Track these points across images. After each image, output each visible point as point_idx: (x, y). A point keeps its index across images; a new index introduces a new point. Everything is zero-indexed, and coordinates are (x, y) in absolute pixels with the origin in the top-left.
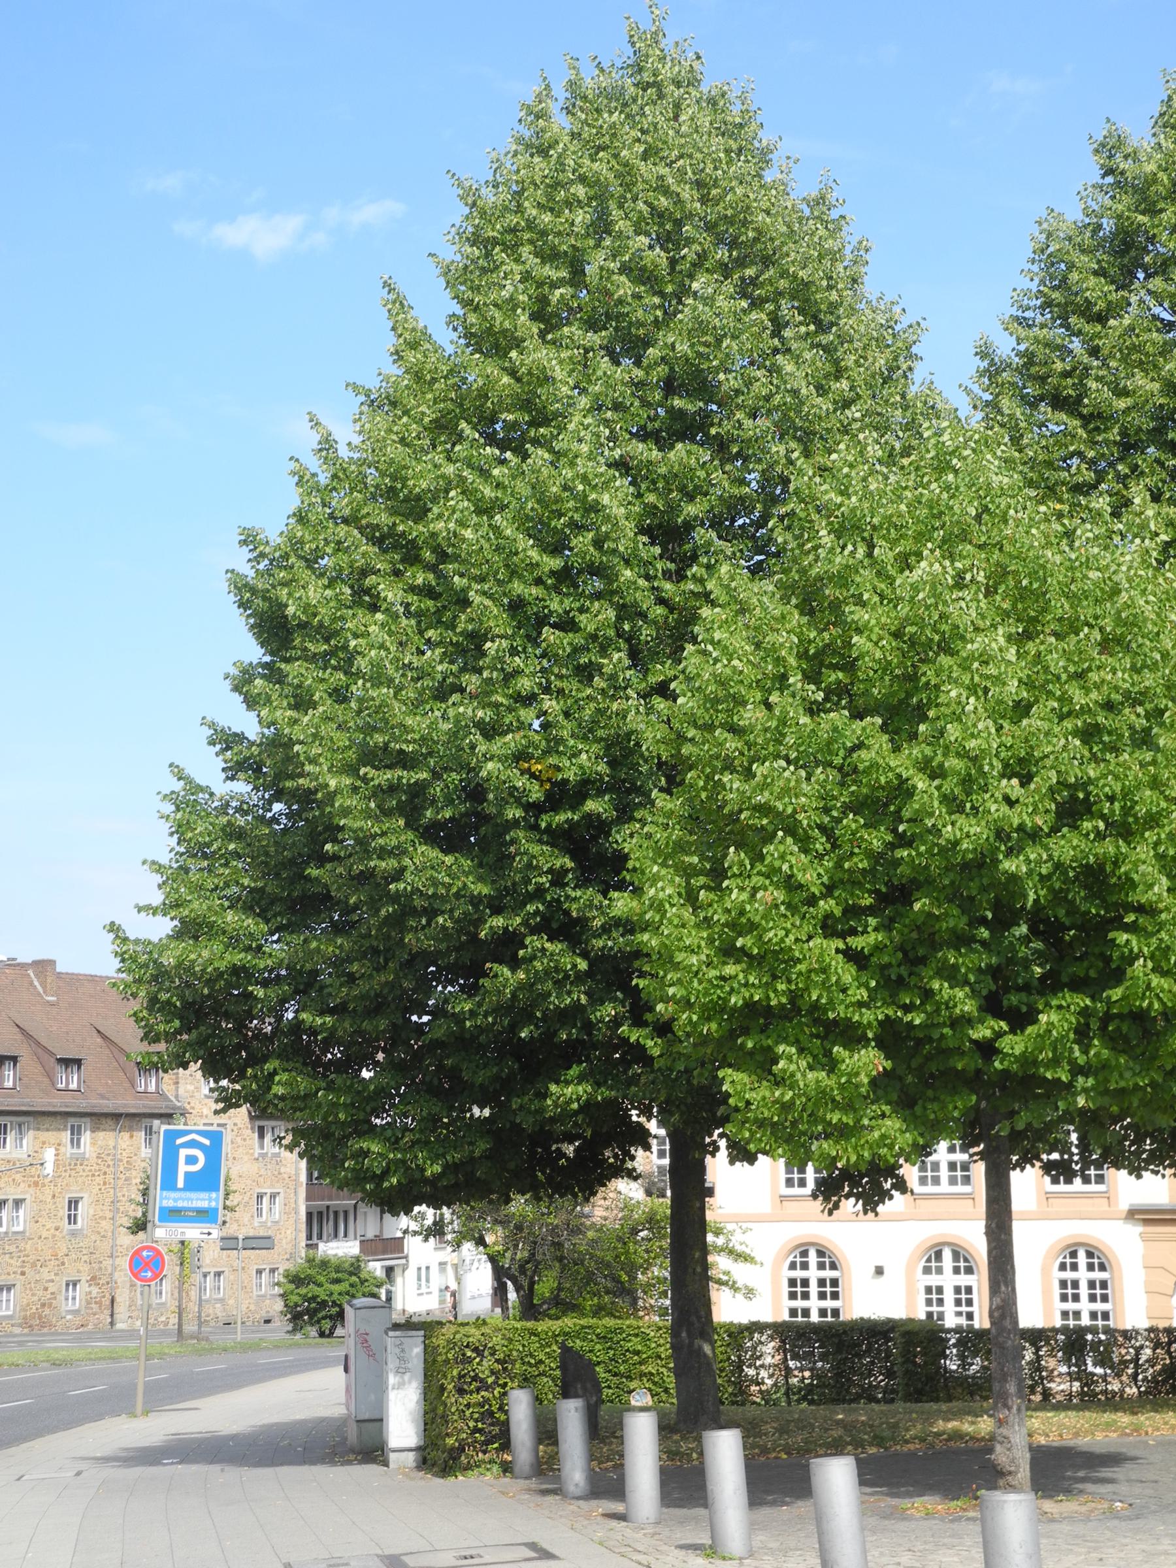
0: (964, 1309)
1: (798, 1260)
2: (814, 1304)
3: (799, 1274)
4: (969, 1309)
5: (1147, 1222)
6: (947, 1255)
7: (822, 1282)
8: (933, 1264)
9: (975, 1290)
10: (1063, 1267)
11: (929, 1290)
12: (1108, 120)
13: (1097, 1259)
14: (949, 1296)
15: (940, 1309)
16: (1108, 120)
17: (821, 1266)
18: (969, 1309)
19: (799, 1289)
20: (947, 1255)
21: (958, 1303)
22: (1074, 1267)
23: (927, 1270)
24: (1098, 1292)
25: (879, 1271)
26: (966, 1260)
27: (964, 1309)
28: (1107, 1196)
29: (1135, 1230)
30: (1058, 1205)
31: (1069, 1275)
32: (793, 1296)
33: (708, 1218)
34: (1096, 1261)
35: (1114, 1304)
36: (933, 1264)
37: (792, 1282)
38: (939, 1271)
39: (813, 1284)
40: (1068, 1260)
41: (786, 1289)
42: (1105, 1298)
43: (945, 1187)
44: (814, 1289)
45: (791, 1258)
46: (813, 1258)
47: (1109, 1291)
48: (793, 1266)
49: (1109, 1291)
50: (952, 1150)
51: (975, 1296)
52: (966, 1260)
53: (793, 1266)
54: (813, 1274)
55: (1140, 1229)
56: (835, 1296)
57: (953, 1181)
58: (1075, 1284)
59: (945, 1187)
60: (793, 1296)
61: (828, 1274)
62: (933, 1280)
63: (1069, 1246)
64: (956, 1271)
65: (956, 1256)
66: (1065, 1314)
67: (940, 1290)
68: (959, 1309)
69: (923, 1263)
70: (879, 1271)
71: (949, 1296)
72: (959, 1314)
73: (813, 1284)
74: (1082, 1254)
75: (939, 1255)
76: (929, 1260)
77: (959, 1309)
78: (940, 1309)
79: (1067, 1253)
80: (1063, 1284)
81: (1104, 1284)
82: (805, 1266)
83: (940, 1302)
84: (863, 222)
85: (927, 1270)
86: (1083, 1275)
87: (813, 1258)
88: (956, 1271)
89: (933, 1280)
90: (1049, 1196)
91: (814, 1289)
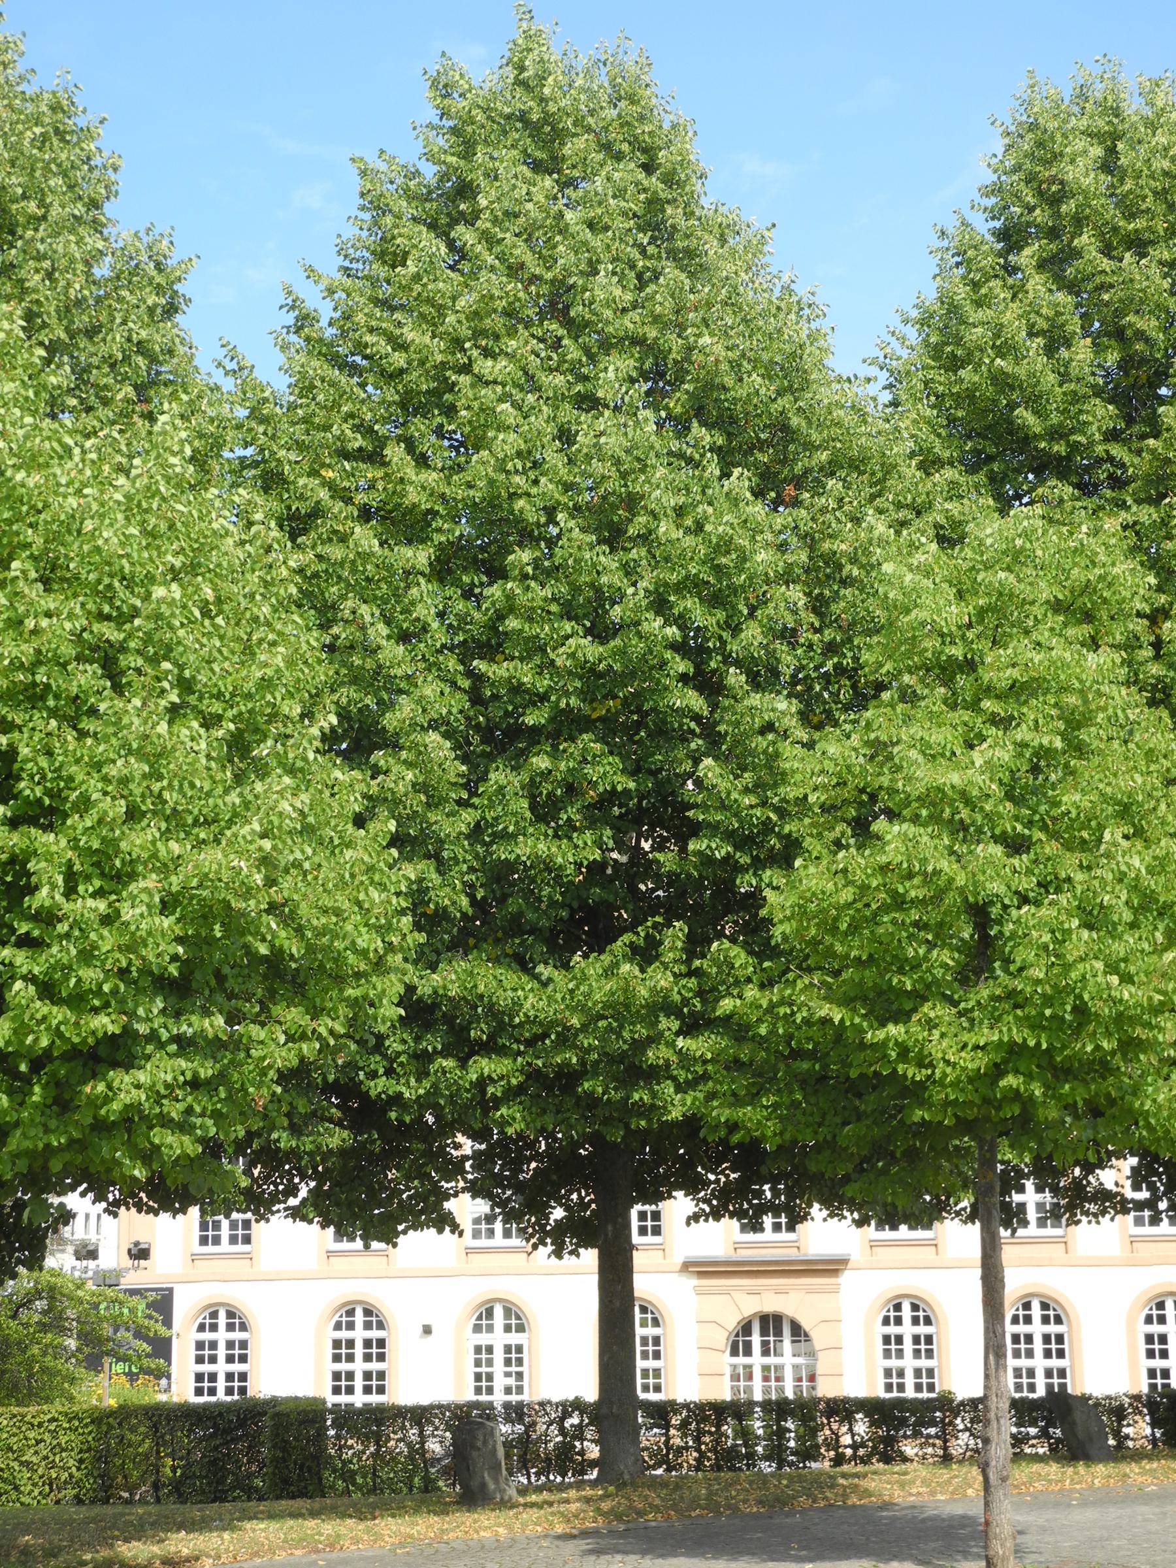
3: (344, 1334)
4: (519, 1369)
5: (701, 1274)
6: (498, 1312)
7: (368, 1343)
8: (484, 1322)
9: (525, 1350)
10: (1149, 1320)
11: (478, 1350)
12: (443, 54)
13: (923, 1314)
14: (499, 1356)
16: (443, 54)
17: (230, 1327)
19: (374, 1350)
20: (498, 1312)
21: (508, 1362)
22: (899, 1321)
23: (477, 1329)
24: (1157, 1347)
25: (427, 1330)
26: (518, 1318)
27: (514, 1369)
29: (690, 1282)
30: (1143, 1249)
31: (893, 1330)
32: (200, 1360)
34: (1051, 1313)
35: (939, 1361)
36: (484, 1322)
37: (337, 1344)
38: (490, 1328)
40: (1155, 1312)
41: (1143, 1347)
42: (1061, 1354)
44: (359, 1351)
45: (336, 1318)
46: (359, 1318)
47: (661, 1348)
48: (338, 1326)
51: (192, 1353)
52: (518, 1318)
53: (338, 1326)
54: (359, 1334)
56: (381, 1358)
57: (233, 1240)
58: (351, 1344)
59: (499, 1240)
60: (1150, 1354)
61: (375, 1334)
62: (483, 1339)
63: (210, 1306)
64: (508, 1329)
65: (508, 1312)
66: (1152, 1373)
67: (490, 1349)
68: (508, 1369)
69: (473, 1321)
70: (427, 1330)
71: (499, 1356)
72: (508, 1375)
74: (222, 1315)
75: (490, 1313)
76: (480, 1318)
77: (508, 1369)
78: (489, 1370)
80: (1149, 1339)
81: (1060, 1339)
82: (351, 1326)
83: (490, 1363)
85: (477, 1329)
86: (907, 1330)
87: (359, 1318)
88: (508, 1329)
89: (483, 1339)
90: (1133, 1240)
91: (359, 1351)
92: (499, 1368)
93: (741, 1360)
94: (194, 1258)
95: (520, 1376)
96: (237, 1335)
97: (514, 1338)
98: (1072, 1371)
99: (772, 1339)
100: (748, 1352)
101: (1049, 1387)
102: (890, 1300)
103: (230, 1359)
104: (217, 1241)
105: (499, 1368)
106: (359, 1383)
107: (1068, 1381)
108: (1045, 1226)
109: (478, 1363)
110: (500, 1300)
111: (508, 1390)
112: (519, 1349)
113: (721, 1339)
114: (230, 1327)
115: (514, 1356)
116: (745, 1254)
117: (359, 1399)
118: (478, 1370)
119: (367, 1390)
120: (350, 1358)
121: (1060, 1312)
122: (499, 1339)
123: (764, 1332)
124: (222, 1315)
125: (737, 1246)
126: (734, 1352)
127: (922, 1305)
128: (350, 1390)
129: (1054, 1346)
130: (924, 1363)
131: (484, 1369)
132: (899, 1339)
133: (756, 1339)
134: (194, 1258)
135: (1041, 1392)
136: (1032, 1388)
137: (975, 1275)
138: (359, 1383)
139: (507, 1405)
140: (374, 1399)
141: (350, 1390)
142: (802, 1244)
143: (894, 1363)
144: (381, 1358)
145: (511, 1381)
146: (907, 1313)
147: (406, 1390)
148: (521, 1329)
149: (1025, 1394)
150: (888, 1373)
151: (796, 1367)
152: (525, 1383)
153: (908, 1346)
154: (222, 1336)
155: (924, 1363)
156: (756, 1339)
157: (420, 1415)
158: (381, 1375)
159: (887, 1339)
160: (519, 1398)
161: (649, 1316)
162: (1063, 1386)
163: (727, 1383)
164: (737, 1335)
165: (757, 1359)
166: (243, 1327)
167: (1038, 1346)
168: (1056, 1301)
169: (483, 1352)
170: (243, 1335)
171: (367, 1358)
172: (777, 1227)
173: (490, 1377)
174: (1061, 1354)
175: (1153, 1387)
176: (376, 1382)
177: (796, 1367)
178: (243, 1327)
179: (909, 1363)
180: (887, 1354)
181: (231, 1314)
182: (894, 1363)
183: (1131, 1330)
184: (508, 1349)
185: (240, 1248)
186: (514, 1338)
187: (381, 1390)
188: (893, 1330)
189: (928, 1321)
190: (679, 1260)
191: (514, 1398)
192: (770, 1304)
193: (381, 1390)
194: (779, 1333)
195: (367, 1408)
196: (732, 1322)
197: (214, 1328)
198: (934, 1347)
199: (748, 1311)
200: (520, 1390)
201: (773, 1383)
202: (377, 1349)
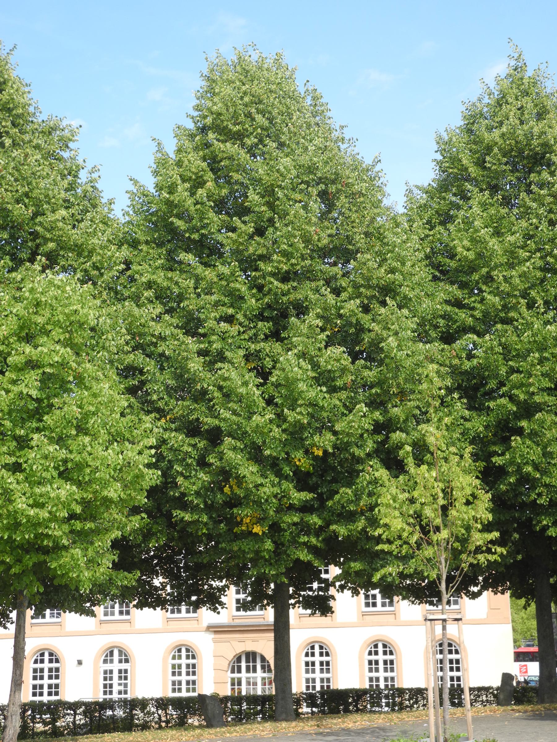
0: (123, 681)
1: (39, 658)
2: (318, 675)
6: (116, 653)
8: (109, 658)
10: (174, 658)
11: (105, 672)
13: (191, 654)
14: (116, 675)
15: (111, 682)
17: (51, 661)
18: (126, 682)
20: (116, 653)
21: (120, 678)
22: (376, 653)
23: (105, 661)
25: (80, 663)
26: (126, 655)
28: (394, 613)
30: (173, 625)
31: (310, 659)
32: (35, 678)
33: (534, 624)
34: (388, 649)
35: (333, 674)
36: (109, 658)
38: (112, 661)
39: (381, 663)
42: (458, 669)
43: (379, 608)
44: (46, 674)
45: (35, 657)
47: (460, 665)
49: (460, 665)
50: (238, 592)
52: (126, 655)
53: (36, 662)
54: (46, 665)
55: (212, 636)
56: (57, 677)
57: (121, 613)
58: (42, 670)
59: (117, 616)
62: (108, 667)
63: (177, 646)
64: (120, 661)
65: (120, 652)
66: (371, 679)
68: (120, 682)
69: (103, 658)
70: (80, 663)
71: (116, 675)
72: (120, 684)
73: (381, 663)
74: (380, 646)
75: (112, 653)
76: (107, 656)
77: (120, 682)
78: (111, 682)
79: (176, 650)
83: (111, 679)
84: (290, 60)
85: (105, 661)
86: (317, 659)
88: (120, 661)
89: (108, 667)
90: (168, 620)
92: (115, 681)
93: (236, 675)
94: (364, 614)
95: (126, 685)
96: (54, 665)
97: (124, 666)
98: (398, 678)
99: (251, 664)
100: (239, 671)
101: (322, 687)
102: (308, 644)
103: (50, 677)
104: (113, 614)
105: (115, 681)
106: (46, 690)
107: (461, 683)
108: (240, 610)
109: (105, 679)
110: (117, 647)
111: (120, 693)
112: (126, 671)
113: (225, 664)
114: (51, 661)
115: (123, 674)
116: (237, 622)
117: (45, 698)
118: (105, 682)
119: (50, 694)
120: (42, 678)
121: (392, 649)
122: (116, 666)
123: (247, 661)
124: (380, 646)
125: (234, 618)
126: (233, 672)
127: (324, 646)
128: (41, 694)
129: (454, 665)
130: (325, 675)
131: (108, 682)
132: (377, 662)
133: (243, 665)
134: (364, 614)
135: (318, 688)
136: (314, 688)
137: (12, 642)
138: (46, 690)
139: (120, 700)
140: (53, 698)
141: (41, 694)
142: (266, 617)
143: (310, 676)
144: (194, 673)
145: (122, 688)
146: (317, 650)
147: (69, 694)
148: (127, 661)
149: (311, 691)
150: (307, 681)
151: (263, 679)
152: (129, 689)
153: (317, 667)
154: (46, 665)
155: (325, 675)
156: (243, 665)
157: (74, 706)
158: (57, 686)
159: (370, 662)
160: (110, 697)
161: (190, 654)
162: (328, 687)
163: (229, 687)
164: (234, 663)
165: (244, 675)
166: (57, 661)
167: (381, 666)
168: (390, 643)
169: (108, 674)
170: (57, 665)
171: (50, 677)
172: (188, 611)
173: (111, 686)
174: (458, 669)
175: (371, 686)
176: (54, 689)
177: (263, 679)
178: (57, 661)
179: (382, 674)
180: (370, 670)
181: (51, 654)
182: (310, 676)
183: (361, 659)
184: (120, 671)
185: (125, 617)
186: (124, 666)
187: (57, 694)
188: (310, 659)
189: (327, 654)
190: (205, 624)
191: (123, 696)
192: (250, 647)
193: (57, 694)
194: (254, 661)
195: (50, 703)
196: (231, 655)
197: (42, 661)
198: (330, 667)
199: (239, 651)
200: (126, 692)
201: (236, 687)
202: (55, 673)
